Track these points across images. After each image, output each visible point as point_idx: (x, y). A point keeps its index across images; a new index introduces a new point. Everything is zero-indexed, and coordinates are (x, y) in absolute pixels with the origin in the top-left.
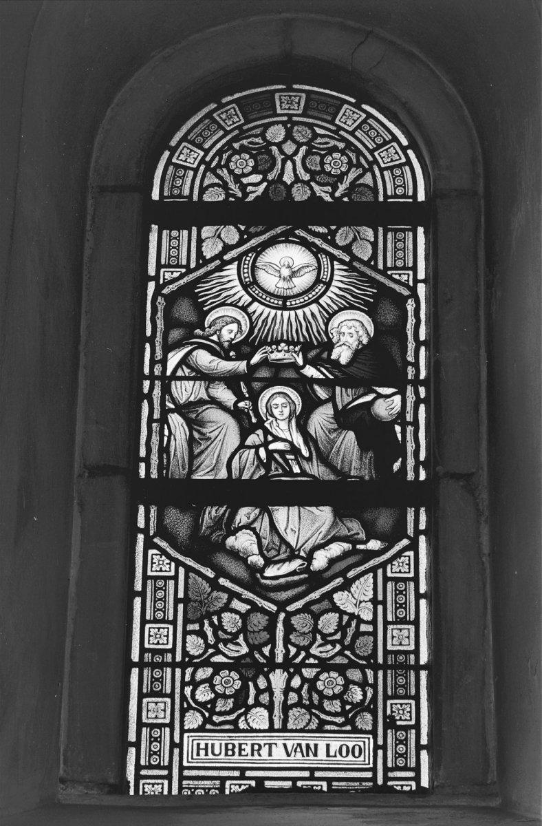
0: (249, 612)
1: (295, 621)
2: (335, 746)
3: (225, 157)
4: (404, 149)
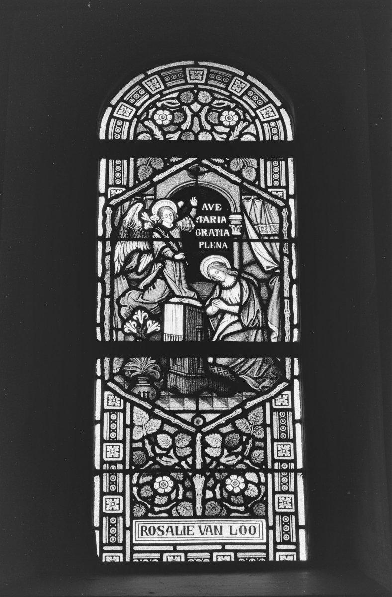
0: (176, 434)
1: (209, 439)
2: (236, 527)
3: (151, 112)
4: (278, 109)
